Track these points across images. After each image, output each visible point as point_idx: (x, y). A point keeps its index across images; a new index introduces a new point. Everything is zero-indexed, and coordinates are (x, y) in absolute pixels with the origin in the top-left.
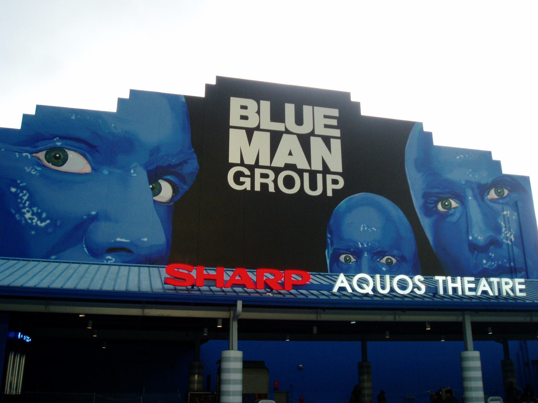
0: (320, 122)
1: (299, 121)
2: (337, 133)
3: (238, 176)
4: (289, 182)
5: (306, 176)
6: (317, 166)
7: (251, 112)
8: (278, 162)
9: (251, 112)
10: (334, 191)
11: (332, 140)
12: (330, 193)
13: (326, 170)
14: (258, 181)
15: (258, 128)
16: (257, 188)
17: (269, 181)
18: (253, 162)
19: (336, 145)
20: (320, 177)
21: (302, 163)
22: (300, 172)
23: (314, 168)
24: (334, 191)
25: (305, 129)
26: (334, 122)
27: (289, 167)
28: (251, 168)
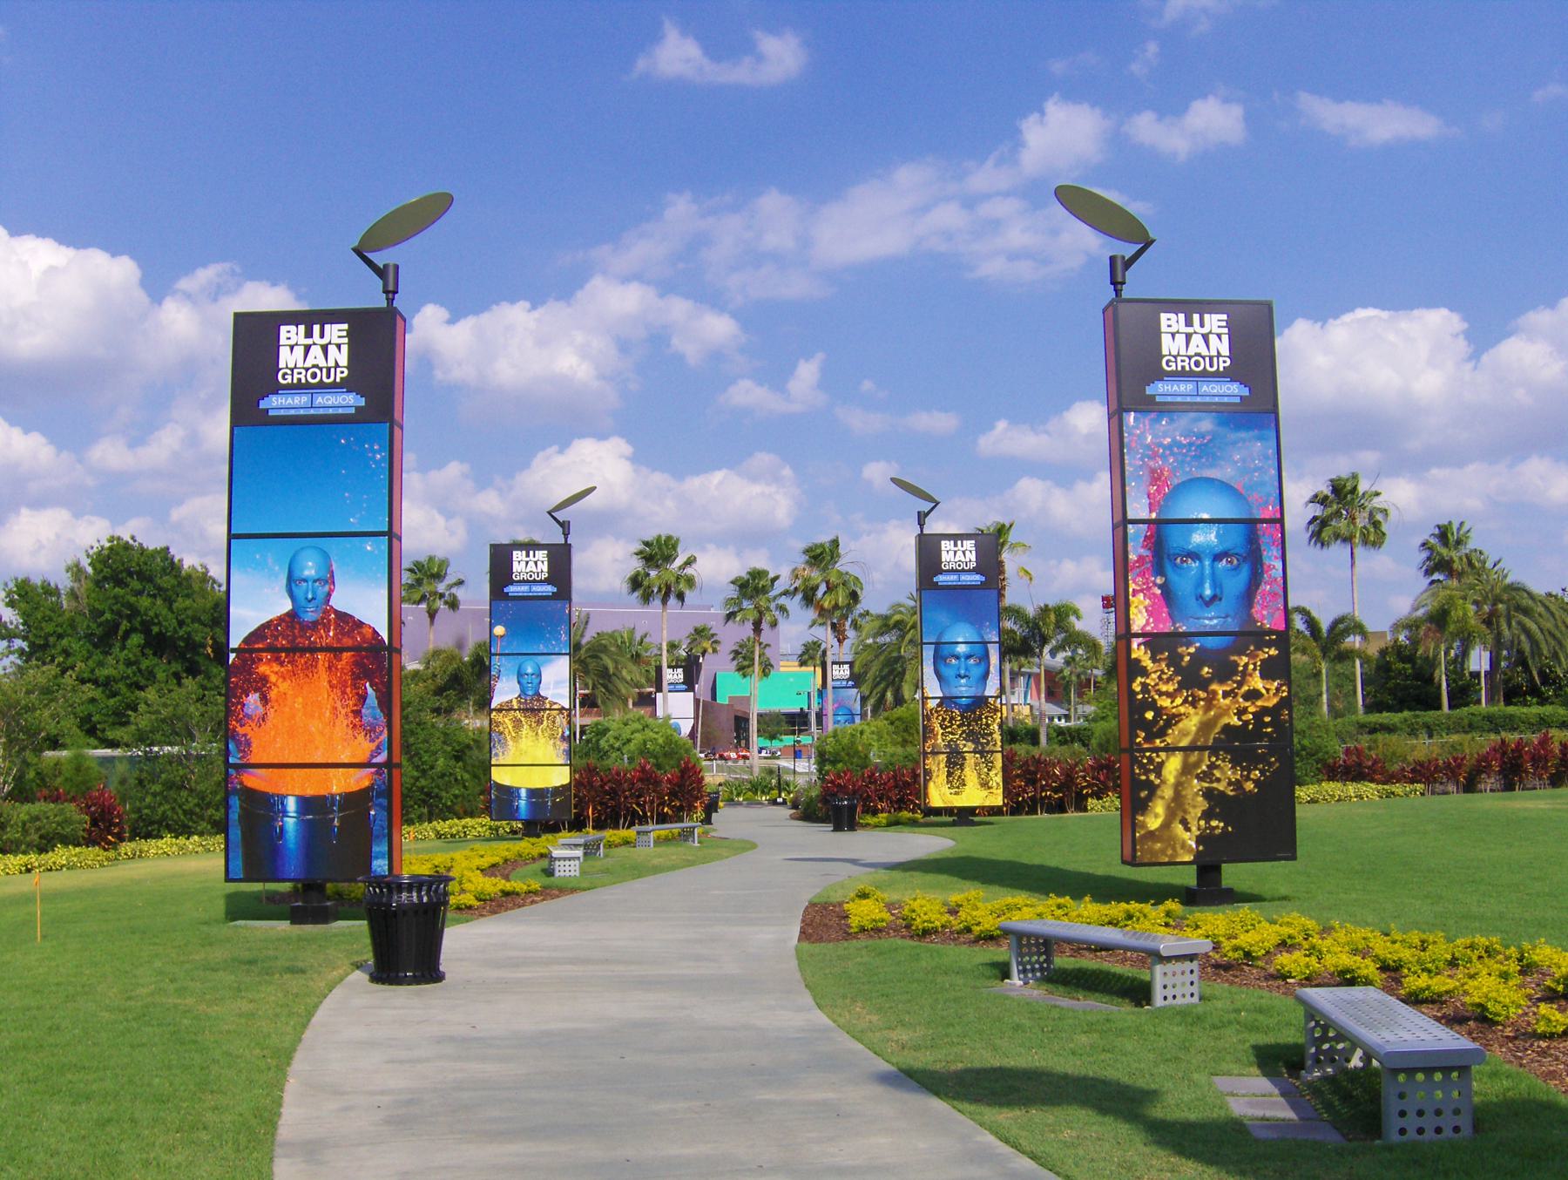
0: (336, 334)
1: (1202, 325)
2: (1226, 330)
3: (1168, 362)
4: (1197, 364)
5: (1207, 359)
6: (331, 363)
7: (1172, 322)
8: (308, 364)
9: (1172, 322)
10: (341, 378)
11: (1223, 336)
12: (1221, 369)
13: (1219, 355)
14: (1180, 364)
15: (1178, 332)
16: (1179, 369)
17: (1186, 364)
18: (1176, 353)
19: (1225, 338)
20: (1215, 359)
21: (1204, 352)
22: (1203, 358)
23: (329, 365)
24: (341, 378)
25: (1205, 331)
26: (1224, 324)
27: (1198, 355)
28: (1175, 357)
